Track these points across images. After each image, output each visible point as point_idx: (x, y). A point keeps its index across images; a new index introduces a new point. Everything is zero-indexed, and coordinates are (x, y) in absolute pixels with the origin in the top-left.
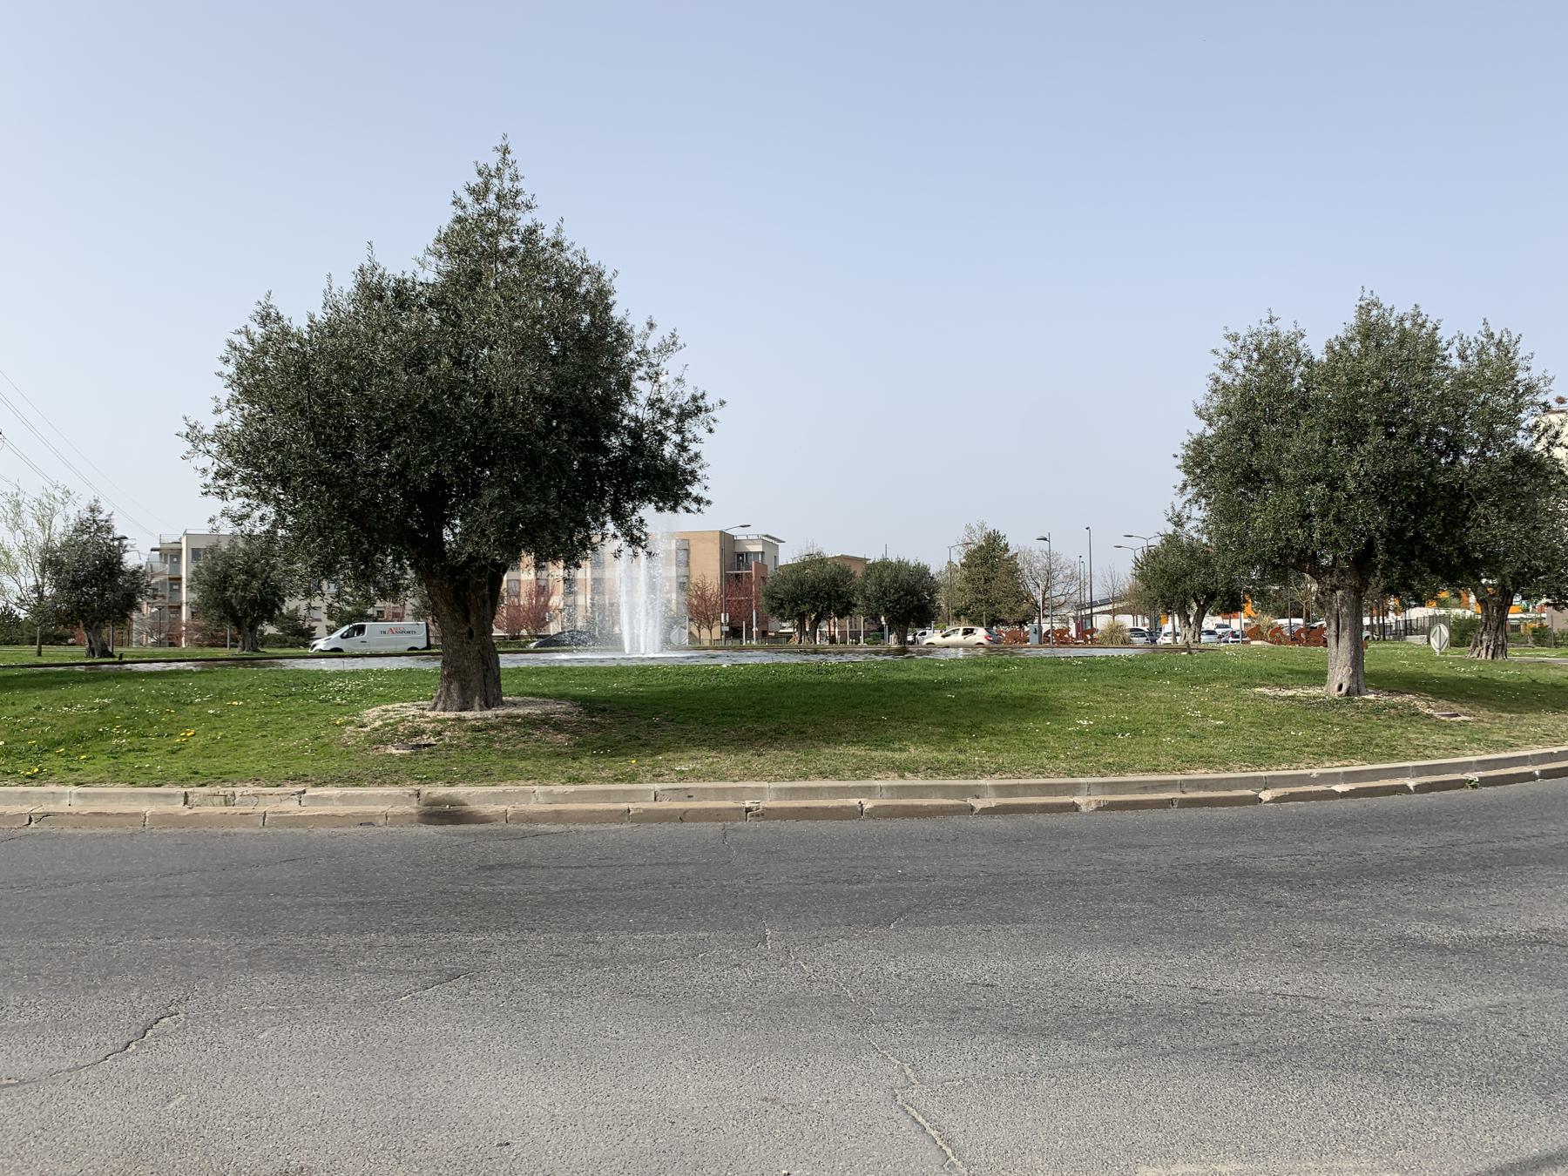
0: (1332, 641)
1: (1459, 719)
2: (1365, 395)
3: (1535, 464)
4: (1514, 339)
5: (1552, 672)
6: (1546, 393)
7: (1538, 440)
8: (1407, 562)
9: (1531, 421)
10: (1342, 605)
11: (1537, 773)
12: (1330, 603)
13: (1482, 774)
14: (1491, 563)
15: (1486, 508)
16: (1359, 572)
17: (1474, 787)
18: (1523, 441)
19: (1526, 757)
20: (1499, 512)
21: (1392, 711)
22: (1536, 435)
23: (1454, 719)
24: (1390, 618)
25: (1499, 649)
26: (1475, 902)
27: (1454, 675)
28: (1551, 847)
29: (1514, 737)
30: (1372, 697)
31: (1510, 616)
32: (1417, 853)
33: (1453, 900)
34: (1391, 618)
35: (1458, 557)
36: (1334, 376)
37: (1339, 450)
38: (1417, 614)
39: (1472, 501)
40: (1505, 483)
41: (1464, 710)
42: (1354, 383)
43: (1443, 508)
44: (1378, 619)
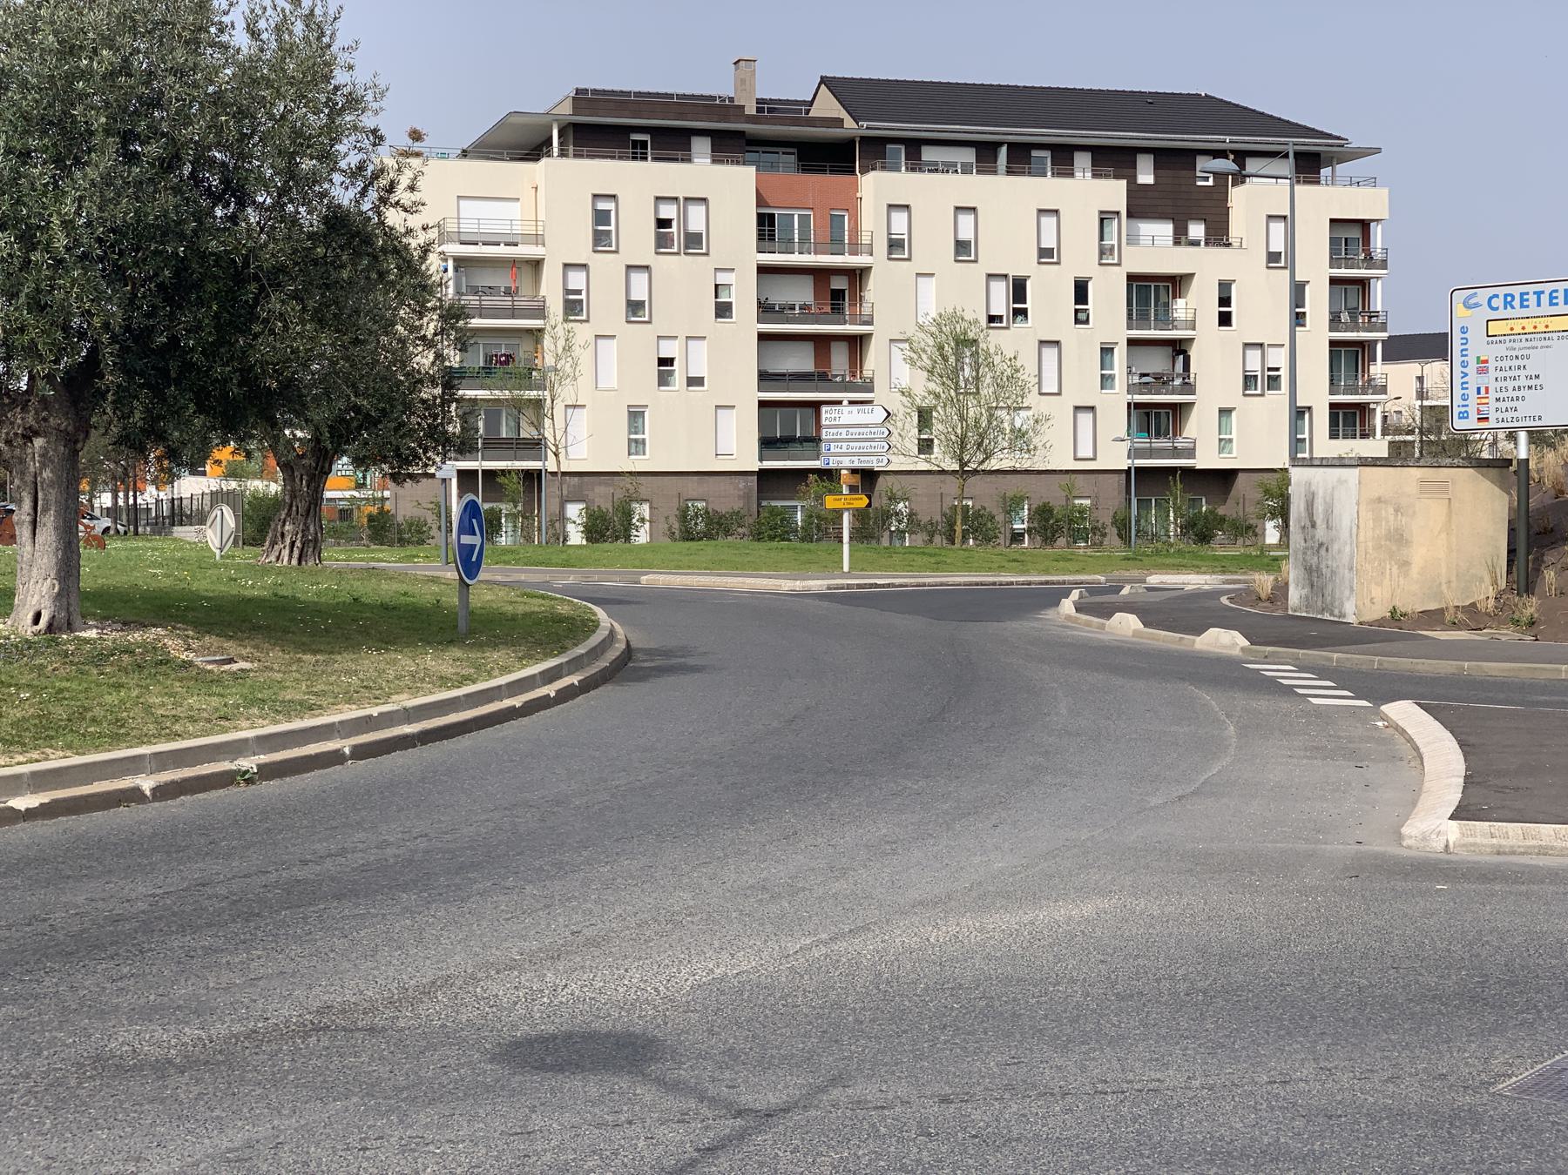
0: (24, 533)
1: (235, 667)
2: (86, 74)
3: (358, 233)
4: (331, 12)
5: (384, 585)
6: (376, 113)
7: (364, 192)
8: (157, 392)
9: (353, 159)
10: (43, 465)
11: (347, 751)
12: (22, 461)
13: (263, 759)
14: (291, 397)
15: (283, 302)
16: (75, 403)
17: (249, 782)
18: (344, 195)
19: (332, 725)
20: (304, 309)
21: (125, 657)
22: (360, 184)
23: (226, 667)
24: (147, 496)
25: (309, 547)
26: (226, 977)
27: (235, 592)
28: (354, 870)
29: (316, 694)
30: (92, 634)
31: (328, 494)
32: (142, 906)
33: (193, 979)
34: (149, 495)
35: (240, 385)
36: (35, 31)
37: (40, 172)
38: (190, 486)
39: (262, 288)
40: (315, 262)
41: (244, 652)
42: (69, 50)
43: (216, 296)
44: (127, 497)
